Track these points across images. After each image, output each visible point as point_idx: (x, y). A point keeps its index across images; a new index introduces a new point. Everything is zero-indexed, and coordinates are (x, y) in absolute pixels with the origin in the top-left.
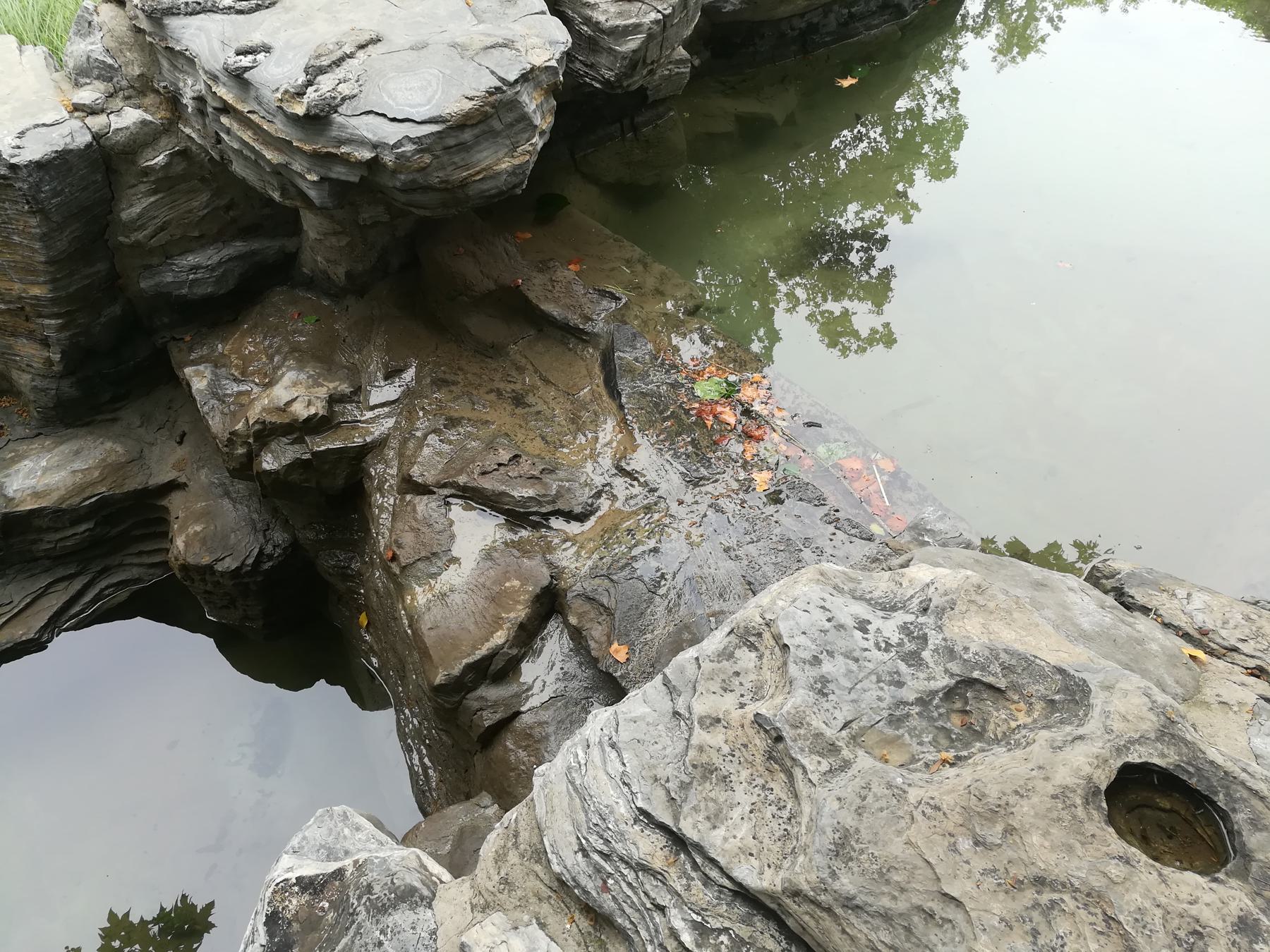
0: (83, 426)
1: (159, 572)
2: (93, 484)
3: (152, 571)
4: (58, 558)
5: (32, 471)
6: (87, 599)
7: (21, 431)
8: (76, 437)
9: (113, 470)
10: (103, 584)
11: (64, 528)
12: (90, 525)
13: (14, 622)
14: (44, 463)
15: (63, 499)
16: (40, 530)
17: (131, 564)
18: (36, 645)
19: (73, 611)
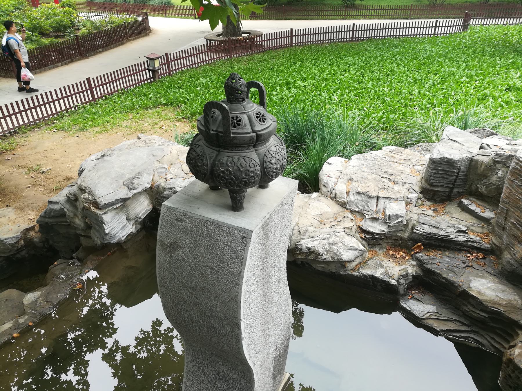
0: (512, 284)
1: (493, 349)
2: (500, 305)
3: (491, 347)
4: (465, 315)
5: (483, 284)
6: (463, 335)
7: (490, 270)
8: (507, 286)
9: (510, 306)
10: (471, 336)
11: (477, 309)
12: (486, 316)
13: (437, 321)
14: (489, 285)
15: (486, 301)
16: (470, 303)
17: (486, 339)
18: (436, 333)
19: (455, 334)
